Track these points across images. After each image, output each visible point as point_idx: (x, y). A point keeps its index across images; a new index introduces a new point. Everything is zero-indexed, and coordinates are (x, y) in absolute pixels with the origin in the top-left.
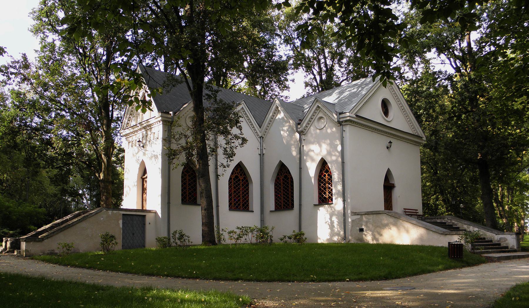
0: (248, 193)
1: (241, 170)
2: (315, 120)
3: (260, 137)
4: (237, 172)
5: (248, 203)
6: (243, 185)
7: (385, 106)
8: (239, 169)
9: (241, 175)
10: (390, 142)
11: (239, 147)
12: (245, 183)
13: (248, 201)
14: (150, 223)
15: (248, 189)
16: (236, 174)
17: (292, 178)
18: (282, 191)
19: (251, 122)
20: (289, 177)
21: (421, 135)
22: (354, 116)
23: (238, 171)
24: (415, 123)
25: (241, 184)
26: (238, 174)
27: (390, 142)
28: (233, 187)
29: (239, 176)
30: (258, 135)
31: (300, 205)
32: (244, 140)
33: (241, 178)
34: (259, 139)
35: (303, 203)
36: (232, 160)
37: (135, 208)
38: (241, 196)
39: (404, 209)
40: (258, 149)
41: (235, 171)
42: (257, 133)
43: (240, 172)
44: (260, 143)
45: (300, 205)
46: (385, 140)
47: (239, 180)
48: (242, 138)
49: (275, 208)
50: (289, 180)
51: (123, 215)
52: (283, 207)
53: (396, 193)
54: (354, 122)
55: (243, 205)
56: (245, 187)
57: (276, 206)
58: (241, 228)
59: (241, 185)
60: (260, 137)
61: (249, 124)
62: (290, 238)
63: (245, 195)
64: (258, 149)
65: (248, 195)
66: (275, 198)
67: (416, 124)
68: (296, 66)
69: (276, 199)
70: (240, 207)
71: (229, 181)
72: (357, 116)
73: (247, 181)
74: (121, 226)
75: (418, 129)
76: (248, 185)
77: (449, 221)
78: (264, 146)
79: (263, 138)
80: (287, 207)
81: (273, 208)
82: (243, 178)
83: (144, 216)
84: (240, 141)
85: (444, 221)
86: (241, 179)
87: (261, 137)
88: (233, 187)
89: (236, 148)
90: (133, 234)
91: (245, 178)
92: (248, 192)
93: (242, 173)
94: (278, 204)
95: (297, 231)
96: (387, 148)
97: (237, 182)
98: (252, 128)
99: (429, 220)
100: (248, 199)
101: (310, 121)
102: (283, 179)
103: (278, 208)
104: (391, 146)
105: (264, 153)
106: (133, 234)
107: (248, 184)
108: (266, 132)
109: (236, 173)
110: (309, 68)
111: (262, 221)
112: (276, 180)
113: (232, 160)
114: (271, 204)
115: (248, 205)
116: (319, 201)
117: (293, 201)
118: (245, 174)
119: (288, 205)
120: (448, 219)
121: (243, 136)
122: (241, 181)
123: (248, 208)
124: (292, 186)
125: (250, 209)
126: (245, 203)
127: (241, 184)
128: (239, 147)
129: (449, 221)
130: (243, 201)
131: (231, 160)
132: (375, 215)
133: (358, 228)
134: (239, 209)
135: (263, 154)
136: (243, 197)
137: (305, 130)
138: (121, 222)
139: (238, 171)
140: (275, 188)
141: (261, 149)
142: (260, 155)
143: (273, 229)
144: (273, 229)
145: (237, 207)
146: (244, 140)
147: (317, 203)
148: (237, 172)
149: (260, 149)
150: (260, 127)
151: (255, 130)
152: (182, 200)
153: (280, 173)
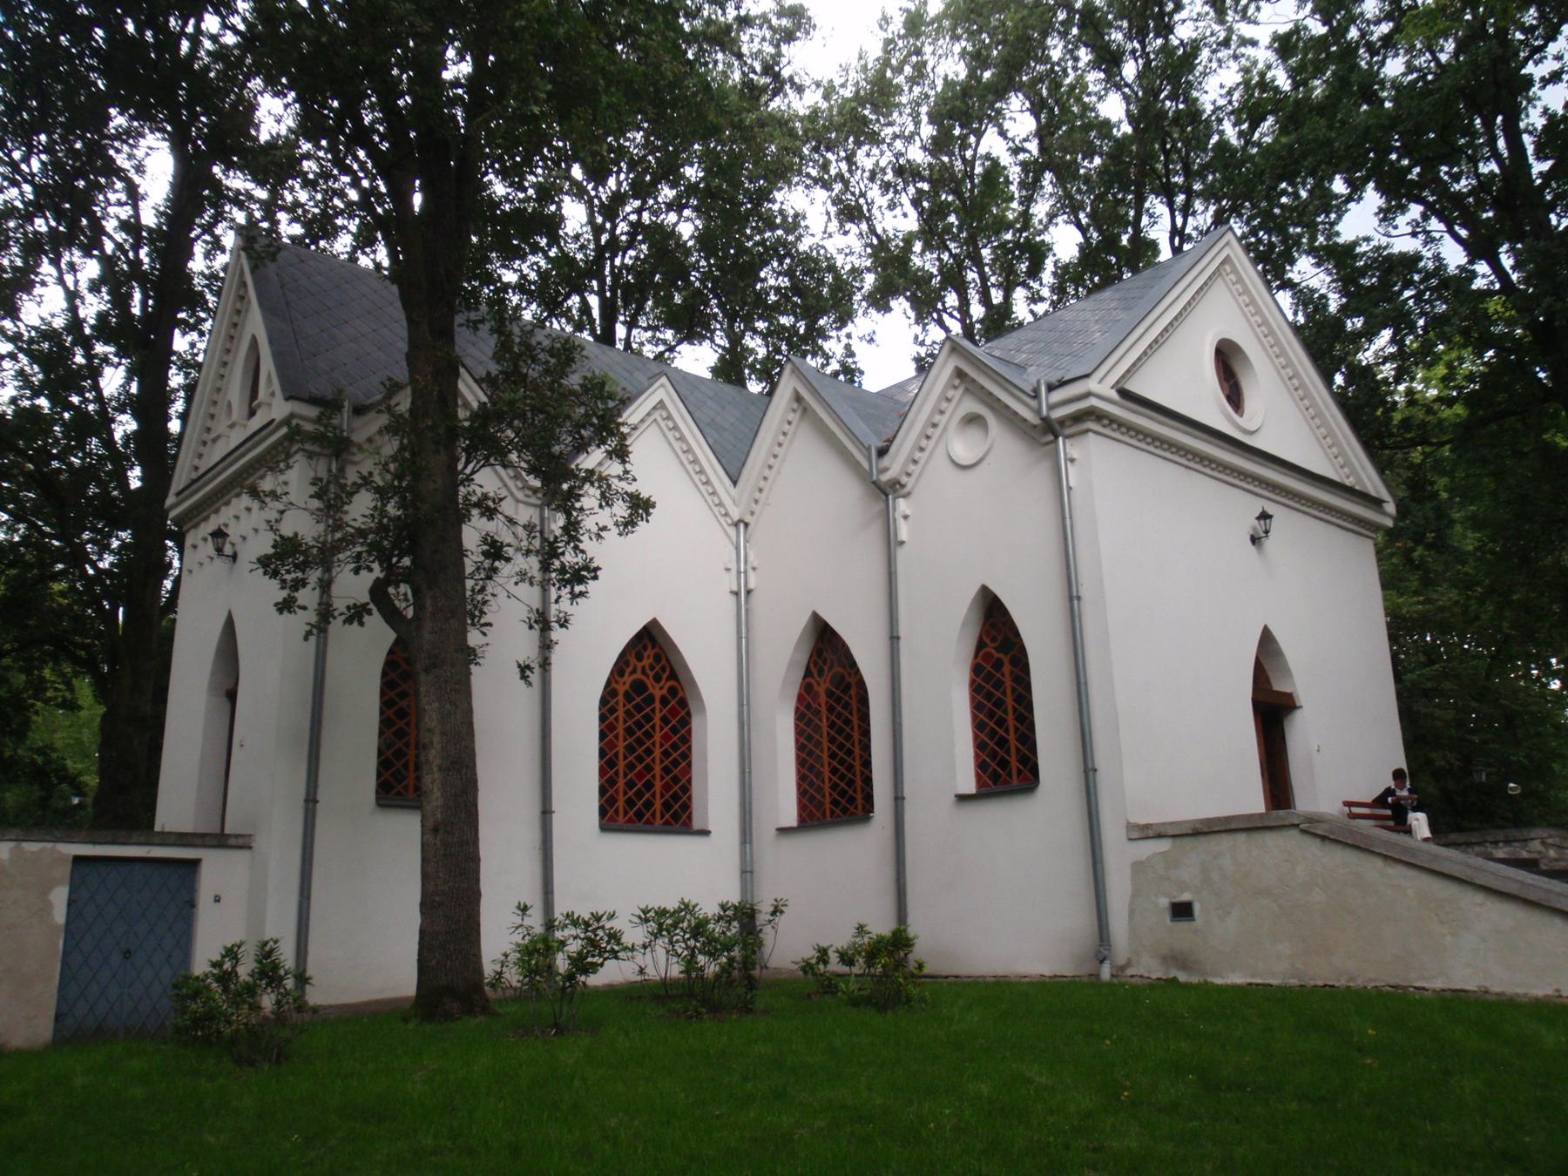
0: (686, 756)
1: (657, 658)
2: (945, 429)
3: (736, 524)
4: (639, 665)
5: (690, 798)
6: (665, 720)
7: (1227, 360)
8: (650, 652)
9: (657, 679)
10: (1264, 516)
11: (612, 535)
12: (673, 712)
13: (686, 789)
14: (217, 899)
15: (686, 739)
16: (638, 675)
17: (861, 684)
18: (825, 740)
19: (695, 461)
20: (852, 680)
21: (1377, 491)
22: (1114, 395)
23: (646, 662)
24: (1349, 444)
25: (658, 715)
26: (644, 672)
27: (1264, 516)
28: (621, 728)
29: (649, 682)
30: (726, 515)
31: (898, 799)
32: (640, 507)
33: (657, 691)
34: (732, 531)
35: (908, 791)
36: (582, 594)
37: (188, 828)
38: (658, 769)
39: (1348, 804)
40: (728, 570)
41: (633, 661)
42: (721, 504)
43: (652, 668)
44: (737, 548)
45: (898, 799)
46: (1246, 506)
47: (651, 699)
48: (631, 496)
49: (800, 815)
50: (853, 692)
51: (78, 860)
52: (832, 812)
53: (1302, 733)
54: (1112, 421)
55: (667, 806)
56: (674, 730)
57: (802, 807)
58: (587, 924)
59: (657, 721)
60: (736, 524)
61: (683, 457)
62: (846, 959)
63: (675, 763)
64: (728, 570)
65: (689, 765)
66: (798, 771)
67: (1353, 450)
68: (880, 300)
69: (802, 778)
70: (653, 815)
71: (604, 701)
72: (1125, 394)
73: (683, 703)
74: (60, 915)
75: (1363, 468)
76: (686, 721)
77: (1552, 853)
78: (751, 557)
79: (746, 525)
80: (845, 811)
81: (790, 817)
82: (665, 691)
83: (195, 863)
84: (621, 509)
85: (1525, 855)
86: (658, 694)
87: (741, 521)
88: (621, 728)
89: (599, 536)
90: (127, 954)
91: (673, 691)
92: (689, 748)
93: (663, 669)
94: (812, 799)
95: (882, 926)
96: (1255, 540)
97: (639, 708)
98: (683, 457)
99: (1477, 849)
100: (689, 781)
101: (928, 437)
102: (830, 694)
103: (811, 816)
104: (1267, 532)
105: (752, 585)
106: (127, 954)
107: (689, 714)
108: (756, 502)
109: (634, 671)
110: (926, 307)
111: (747, 872)
112: (800, 699)
113: (582, 594)
114: (782, 799)
115: (687, 807)
116: (978, 777)
117: (868, 781)
118: (673, 676)
119: (852, 800)
120: (1543, 843)
121: (631, 489)
122: (657, 705)
123: (690, 817)
124: (865, 718)
125: (696, 825)
126: (676, 797)
127: (658, 715)
128: (612, 535)
129: (1552, 853)
130: (666, 787)
131: (574, 596)
132: (1242, 837)
133: (1164, 902)
134: (648, 822)
135: (748, 592)
136: (666, 770)
137: (908, 475)
138: (59, 897)
139: (646, 662)
140: (799, 732)
141: (739, 573)
142: (737, 594)
143: (776, 911)
144: (776, 911)
145: (639, 815)
146: (640, 507)
147: (969, 785)
148: (639, 665)
149: (734, 572)
150: (735, 483)
151: (714, 493)
152: (603, 812)
153: (815, 664)
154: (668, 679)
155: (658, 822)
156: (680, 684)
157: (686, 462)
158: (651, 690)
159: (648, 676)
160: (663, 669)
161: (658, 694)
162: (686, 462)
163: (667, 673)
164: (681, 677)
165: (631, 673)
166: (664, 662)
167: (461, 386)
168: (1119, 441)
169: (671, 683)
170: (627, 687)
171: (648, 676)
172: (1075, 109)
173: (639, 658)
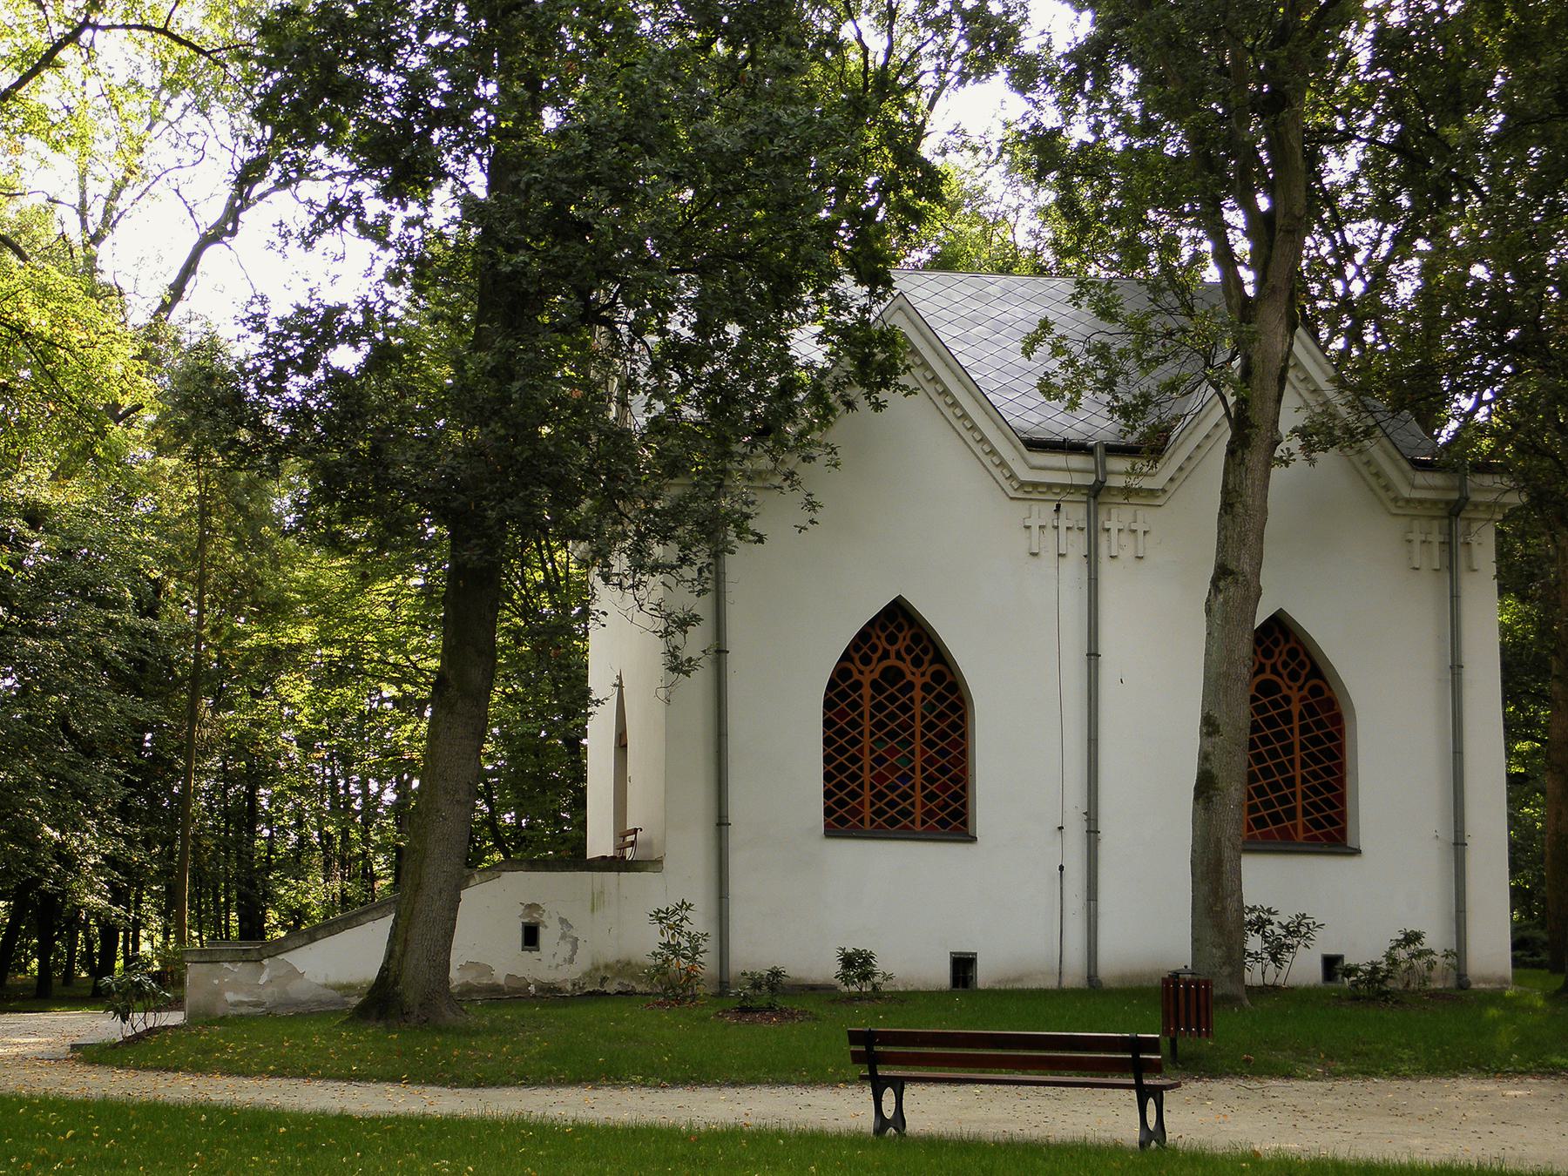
4: (1268, 663)
9: (917, 662)
23: (901, 645)
29: (907, 667)
86: (918, 682)
91: (1316, 691)
109: (886, 655)
115: (1343, 832)
139: (901, 645)
154: (932, 663)
155: (918, 828)
156: (1326, 682)
157: (981, 455)
158: (909, 677)
159: (1280, 675)
160: (1302, 665)
161: (918, 682)
162: (981, 455)
163: (930, 656)
164: (1325, 672)
165: (880, 659)
166: (1302, 656)
167: (1241, 275)
168: (1364, 479)
169: (936, 667)
170: (876, 675)
171: (1280, 675)
172: (565, 347)
173: (892, 639)
